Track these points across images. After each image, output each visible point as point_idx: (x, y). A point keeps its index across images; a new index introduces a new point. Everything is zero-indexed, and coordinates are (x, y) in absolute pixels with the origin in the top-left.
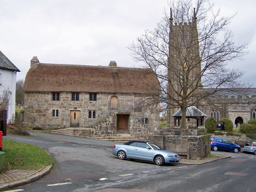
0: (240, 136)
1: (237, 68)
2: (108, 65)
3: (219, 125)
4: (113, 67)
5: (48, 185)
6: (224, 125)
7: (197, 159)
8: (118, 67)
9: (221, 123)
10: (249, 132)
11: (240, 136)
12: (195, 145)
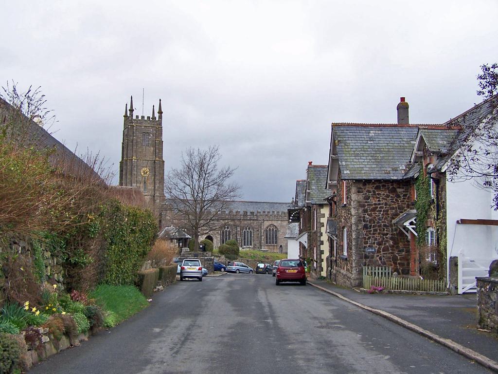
3: (201, 246)
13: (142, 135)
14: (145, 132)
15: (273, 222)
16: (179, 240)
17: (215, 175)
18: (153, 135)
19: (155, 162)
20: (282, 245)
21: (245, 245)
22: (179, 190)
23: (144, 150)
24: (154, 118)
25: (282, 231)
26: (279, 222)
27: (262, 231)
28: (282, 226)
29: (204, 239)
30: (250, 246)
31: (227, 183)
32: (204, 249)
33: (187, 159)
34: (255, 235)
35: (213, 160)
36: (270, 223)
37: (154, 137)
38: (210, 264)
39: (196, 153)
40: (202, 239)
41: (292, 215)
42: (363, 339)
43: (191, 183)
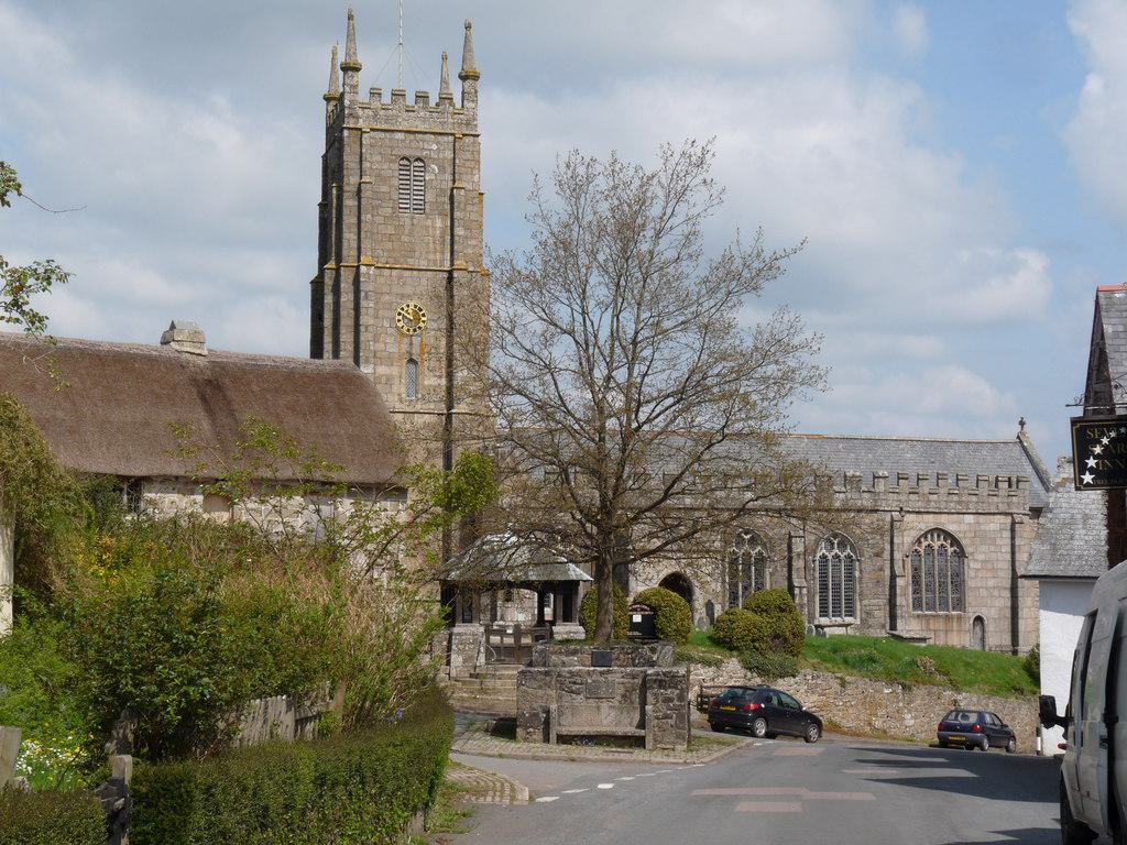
0: (718, 664)
1: (20, 194)
2: (155, 341)
3: (637, 618)
4: (188, 349)
5: (554, 798)
6: (655, 616)
7: (679, 747)
8: (209, 350)
9: (642, 610)
10: (754, 647)
11: (718, 664)
12: (671, 700)
13: (396, 166)
14: (406, 153)
15: (944, 518)
16: (543, 589)
17: (693, 274)
18: (442, 169)
19: (450, 279)
20: (984, 613)
21: (824, 613)
22: (520, 354)
23: (407, 227)
24: (446, 99)
25: (981, 557)
26: (969, 519)
27: (898, 556)
28: (982, 537)
29: (655, 584)
30: (848, 620)
31: (749, 318)
32: (651, 631)
33: (558, 206)
34: (869, 572)
35: (682, 209)
36: (929, 521)
37: (448, 177)
38: (668, 700)
39: (602, 183)
40: (646, 579)
41: (1098, 450)
42: (800, 707)
43: (579, 318)
